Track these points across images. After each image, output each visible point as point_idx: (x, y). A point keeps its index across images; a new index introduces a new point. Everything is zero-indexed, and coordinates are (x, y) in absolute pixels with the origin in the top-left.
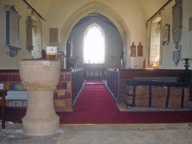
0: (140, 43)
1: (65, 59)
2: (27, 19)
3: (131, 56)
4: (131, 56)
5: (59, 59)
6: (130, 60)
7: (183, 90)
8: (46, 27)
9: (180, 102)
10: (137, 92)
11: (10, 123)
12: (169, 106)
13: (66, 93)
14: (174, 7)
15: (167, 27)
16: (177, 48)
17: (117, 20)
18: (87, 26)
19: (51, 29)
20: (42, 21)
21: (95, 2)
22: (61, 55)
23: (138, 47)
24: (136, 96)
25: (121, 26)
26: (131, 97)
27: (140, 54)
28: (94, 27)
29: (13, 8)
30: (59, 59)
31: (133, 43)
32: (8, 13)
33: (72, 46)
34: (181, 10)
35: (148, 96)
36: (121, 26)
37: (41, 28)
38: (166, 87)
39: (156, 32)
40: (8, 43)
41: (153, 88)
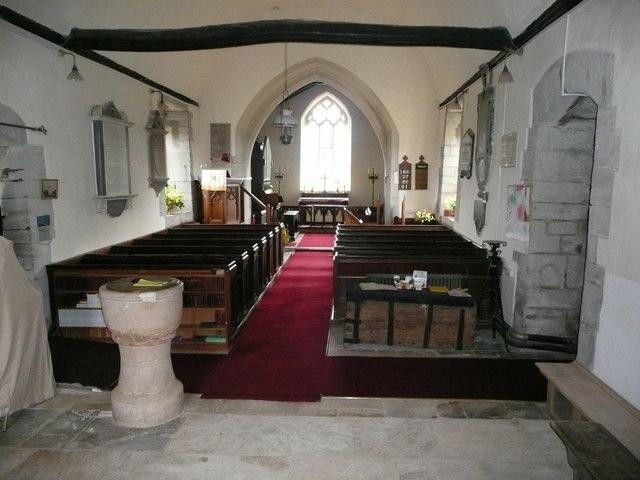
0: (422, 158)
2: (150, 119)
3: (400, 188)
4: (400, 188)
5: (232, 196)
6: (397, 198)
7: (463, 312)
8: (203, 120)
11: (95, 390)
12: (430, 345)
13: (217, 316)
18: (315, 96)
19: (213, 125)
20: (191, 107)
23: (417, 168)
25: (379, 118)
26: (352, 325)
27: (422, 184)
28: (327, 103)
29: (111, 111)
30: (232, 196)
31: (405, 158)
32: (98, 126)
33: (268, 156)
35: (387, 323)
36: (379, 118)
37: (190, 127)
38: (424, 306)
40: (102, 190)
41: (398, 307)
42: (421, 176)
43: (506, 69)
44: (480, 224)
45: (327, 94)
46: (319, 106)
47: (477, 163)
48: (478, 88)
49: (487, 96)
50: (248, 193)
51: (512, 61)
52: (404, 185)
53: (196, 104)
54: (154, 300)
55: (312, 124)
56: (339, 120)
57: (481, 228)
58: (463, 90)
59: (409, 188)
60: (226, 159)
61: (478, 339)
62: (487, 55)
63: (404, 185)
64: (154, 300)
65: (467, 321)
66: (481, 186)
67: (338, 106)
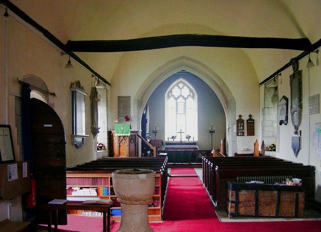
0: (250, 116)
1: (140, 140)
3: (238, 135)
4: (238, 135)
5: (132, 141)
7: (297, 195)
9: (294, 210)
10: (241, 199)
14: (292, 77)
15: (284, 101)
16: (296, 133)
17: (216, 83)
21: (183, 57)
22: (135, 136)
23: (248, 122)
24: (239, 202)
29: (78, 84)
31: (240, 116)
33: (148, 117)
34: (300, 83)
38: (275, 192)
39: (272, 98)
41: (261, 194)
42: (248, 127)
43: (310, 61)
44: (297, 150)
45: (181, 79)
46: (176, 88)
47: (292, 114)
48: (290, 71)
49: (297, 78)
50: (140, 137)
51: (313, 55)
52: (240, 133)
53: (109, 84)
54: (145, 178)
55: (172, 98)
56: (189, 95)
57: (298, 152)
58: (278, 72)
59: (243, 135)
60: (127, 119)
61: (305, 213)
62: (296, 53)
63: (240, 133)
64: (145, 178)
65: (300, 200)
66: (296, 128)
67: (188, 87)
